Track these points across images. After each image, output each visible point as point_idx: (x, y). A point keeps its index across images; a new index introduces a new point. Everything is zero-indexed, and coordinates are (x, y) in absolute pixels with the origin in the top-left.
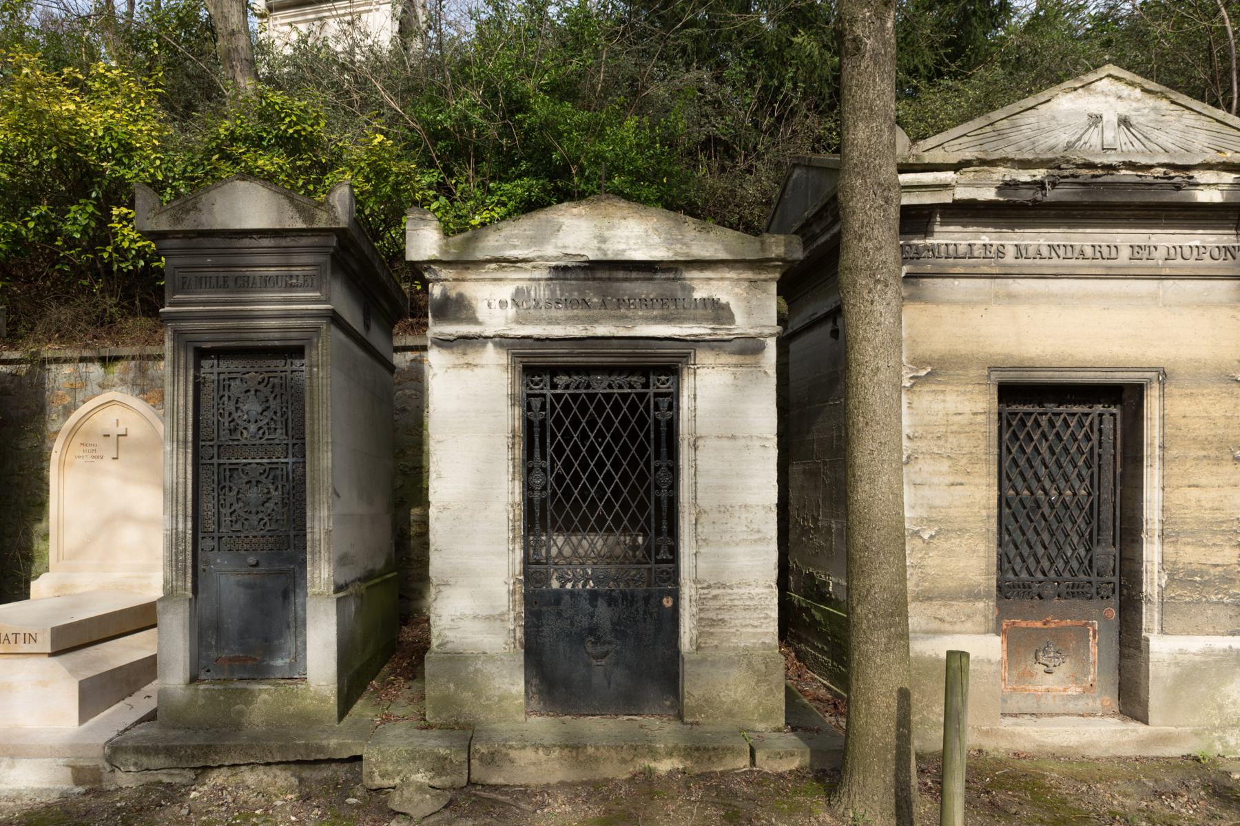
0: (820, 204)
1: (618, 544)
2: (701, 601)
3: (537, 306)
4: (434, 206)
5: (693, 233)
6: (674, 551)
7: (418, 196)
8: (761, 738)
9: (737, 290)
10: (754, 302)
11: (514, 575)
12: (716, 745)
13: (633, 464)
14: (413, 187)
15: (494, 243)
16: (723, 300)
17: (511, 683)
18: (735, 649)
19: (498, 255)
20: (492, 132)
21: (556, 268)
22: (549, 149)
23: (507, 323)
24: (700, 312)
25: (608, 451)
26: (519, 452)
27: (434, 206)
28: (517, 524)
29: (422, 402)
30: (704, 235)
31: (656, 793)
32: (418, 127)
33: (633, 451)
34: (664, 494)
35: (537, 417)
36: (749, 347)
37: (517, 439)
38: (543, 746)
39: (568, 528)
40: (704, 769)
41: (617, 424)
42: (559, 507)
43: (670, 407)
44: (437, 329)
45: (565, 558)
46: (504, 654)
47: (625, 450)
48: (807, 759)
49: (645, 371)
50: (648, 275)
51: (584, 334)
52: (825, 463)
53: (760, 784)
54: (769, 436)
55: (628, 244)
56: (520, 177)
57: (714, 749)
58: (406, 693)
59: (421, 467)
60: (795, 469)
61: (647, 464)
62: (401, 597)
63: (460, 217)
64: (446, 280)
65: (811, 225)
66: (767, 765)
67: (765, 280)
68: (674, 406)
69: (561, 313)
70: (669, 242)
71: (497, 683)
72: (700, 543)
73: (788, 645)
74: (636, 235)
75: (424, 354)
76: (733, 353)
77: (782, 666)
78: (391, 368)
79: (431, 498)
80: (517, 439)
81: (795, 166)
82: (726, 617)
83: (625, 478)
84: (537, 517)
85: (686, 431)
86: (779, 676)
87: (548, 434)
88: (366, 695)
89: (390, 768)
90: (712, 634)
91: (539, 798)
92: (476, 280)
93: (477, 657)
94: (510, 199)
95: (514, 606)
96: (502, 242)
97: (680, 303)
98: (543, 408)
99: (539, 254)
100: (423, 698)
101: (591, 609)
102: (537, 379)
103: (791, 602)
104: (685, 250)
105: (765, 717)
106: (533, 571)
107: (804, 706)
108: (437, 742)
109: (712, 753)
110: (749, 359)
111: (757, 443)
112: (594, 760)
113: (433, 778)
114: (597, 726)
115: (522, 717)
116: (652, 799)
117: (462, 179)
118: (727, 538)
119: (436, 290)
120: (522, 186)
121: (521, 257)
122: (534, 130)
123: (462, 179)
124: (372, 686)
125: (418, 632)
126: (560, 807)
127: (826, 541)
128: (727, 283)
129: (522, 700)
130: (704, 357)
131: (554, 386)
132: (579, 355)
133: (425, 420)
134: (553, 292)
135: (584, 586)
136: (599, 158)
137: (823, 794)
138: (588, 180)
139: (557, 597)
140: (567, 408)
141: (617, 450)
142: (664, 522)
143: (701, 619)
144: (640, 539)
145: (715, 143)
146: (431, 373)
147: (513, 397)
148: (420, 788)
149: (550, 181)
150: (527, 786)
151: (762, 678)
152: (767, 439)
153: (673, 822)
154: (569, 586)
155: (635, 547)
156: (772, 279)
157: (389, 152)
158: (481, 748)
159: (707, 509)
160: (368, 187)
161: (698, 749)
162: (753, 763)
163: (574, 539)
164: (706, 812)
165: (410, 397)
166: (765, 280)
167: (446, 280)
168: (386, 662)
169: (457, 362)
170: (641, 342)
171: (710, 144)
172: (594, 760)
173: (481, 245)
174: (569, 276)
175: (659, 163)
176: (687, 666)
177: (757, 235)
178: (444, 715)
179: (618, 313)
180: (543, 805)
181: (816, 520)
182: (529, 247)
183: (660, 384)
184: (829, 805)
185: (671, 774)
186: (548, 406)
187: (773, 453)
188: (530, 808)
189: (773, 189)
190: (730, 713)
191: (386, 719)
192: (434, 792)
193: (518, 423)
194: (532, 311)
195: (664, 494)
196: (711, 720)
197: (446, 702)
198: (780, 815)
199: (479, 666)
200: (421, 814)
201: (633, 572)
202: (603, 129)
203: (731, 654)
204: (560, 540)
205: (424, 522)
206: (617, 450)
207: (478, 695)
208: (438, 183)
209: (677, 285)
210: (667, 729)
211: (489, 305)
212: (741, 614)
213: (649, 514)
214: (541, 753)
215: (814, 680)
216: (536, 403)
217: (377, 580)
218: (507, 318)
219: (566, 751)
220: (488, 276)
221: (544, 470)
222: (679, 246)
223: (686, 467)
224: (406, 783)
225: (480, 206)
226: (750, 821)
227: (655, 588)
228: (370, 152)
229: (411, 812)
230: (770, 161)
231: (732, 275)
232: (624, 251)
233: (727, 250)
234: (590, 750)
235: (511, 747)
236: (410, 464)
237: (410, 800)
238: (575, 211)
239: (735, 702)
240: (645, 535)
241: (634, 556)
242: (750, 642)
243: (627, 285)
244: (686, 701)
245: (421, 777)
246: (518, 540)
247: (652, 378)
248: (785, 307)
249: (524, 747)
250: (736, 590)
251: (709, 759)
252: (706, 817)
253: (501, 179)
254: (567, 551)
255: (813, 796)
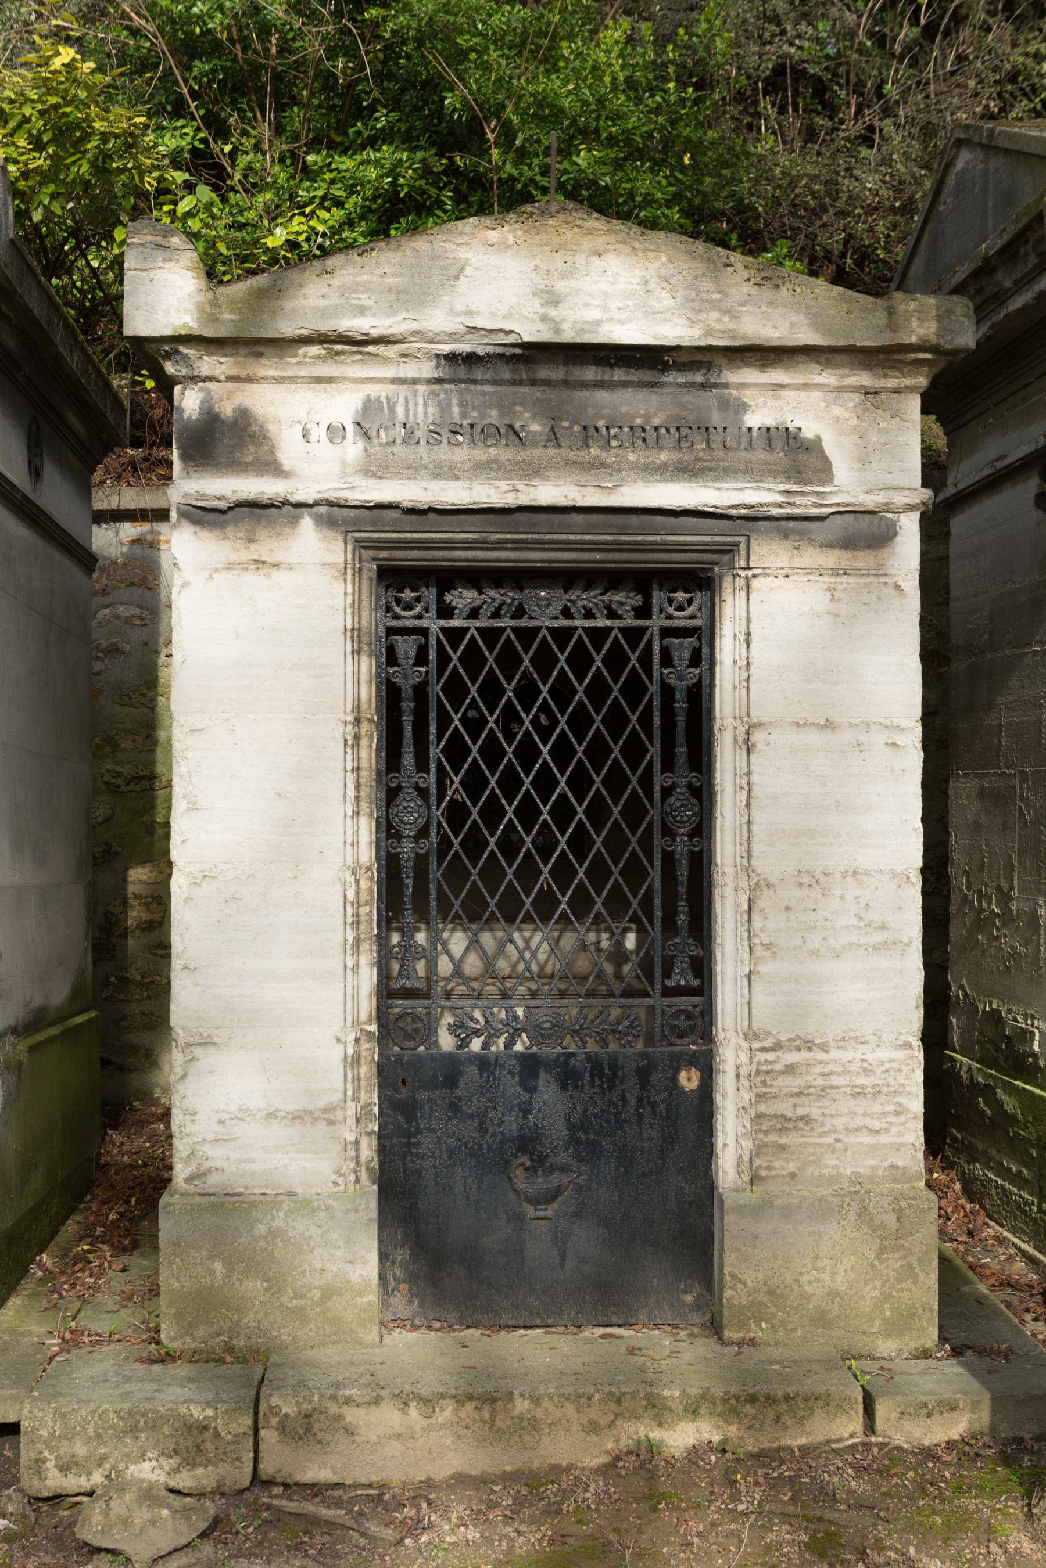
0: (1013, 229)
1: (583, 947)
2: (760, 1079)
3: (410, 437)
4: (185, 205)
5: (746, 288)
6: (702, 968)
7: (150, 182)
8: (888, 1374)
9: (837, 411)
10: (874, 437)
11: (356, 1022)
12: (791, 1390)
13: (616, 782)
14: (138, 167)
15: (318, 299)
16: (809, 433)
17: (344, 1259)
18: (831, 1180)
19: (324, 326)
20: (312, 46)
21: (452, 358)
22: (435, 86)
23: (344, 474)
24: (759, 456)
25: (562, 752)
26: (368, 754)
27: (185, 205)
28: (364, 910)
29: (155, 633)
30: (767, 293)
31: (663, 1497)
32: (151, 27)
33: (616, 753)
34: (681, 846)
35: (408, 678)
36: (863, 533)
37: (365, 727)
38: (419, 1398)
39: (474, 914)
40: (766, 1443)
41: (580, 694)
42: (455, 874)
43: (695, 659)
44: (190, 485)
45: (466, 980)
46: (335, 1196)
47: (598, 751)
48: (984, 1417)
49: (643, 581)
50: (647, 376)
51: (510, 500)
52: (1024, 776)
53: (884, 1473)
54: (904, 723)
55: (605, 308)
56: (372, 142)
57: (788, 1398)
58: (116, 1281)
59: (153, 777)
60: (963, 788)
61: (646, 781)
62: (105, 1063)
63: (239, 227)
64: (211, 379)
65: (993, 270)
66: (899, 1429)
67: (897, 391)
68: (702, 656)
69: (460, 454)
70: (696, 305)
71: (317, 1259)
72: (758, 951)
73: (948, 1166)
74: (624, 289)
75: (162, 527)
76: (830, 545)
77: (934, 1214)
78: (86, 559)
79: (175, 855)
80: (365, 727)
81: (960, 143)
82: (815, 1112)
83: (598, 812)
84: (405, 892)
85: (728, 711)
86: (925, 1238)
87: (433, 715)
88: (27, 1286)
89: (80, 1450)
90: (783, 1148)
91: (409, 1512)
92: (278, 380)
93: (274, 1203)
94: (351, 190)
95: (357, 1090)
96: (334, 300)
97: (717, 437)
98: (421, 658)
99: (415, 326)
100: (154, 1291)
101: (525, 1096)
102: (408, 595)
103: (953, 1074)
104: (728, 323)
105: (896, 1327)
106: (400, 1005)
107: (980, 1301)
108: (186, 1392)
109: (783, 1407)
110: (863, 559)
111: (879, 738)
112: (530, 1425)
113: (175, 1471)
114: (539, 1352)
115: (372, 1334)
116: (654, 1509)
117: (248, 143)
118: (815, 940)
119: (189, 402)
120: (377, 163)
121: (375, 333)
122: (404, 43)
123: (248, 143)
124: (41, 1266)
125: (142, 1143)
126: (453, 1529)
127: (1026, 942)
128: (816, 395)
129: (372, 1297)
130: (767, 553)
131: (446, 611)
132: (500, 545)
133: (163, 673)
134: (444, 409)
135: (509, 1045)
136: (546, 112)
137: (1018, 1491)
138: (522, 155)
139: (450, 1070)
140: (472, 659)
141: (580, 750)
142: (683, 907)
143: (760, 1116)
144: (630, 941)
145: (795, 80)
146: (177, 581)
147: (355, 634)
148: (148, 1495)
149: (440, 155)
150: (383, 1486)
151: (890, 1241)
152: (900, 729)
153: (697, 1559)
154: (476, 1045)
155: (619, 956)
156: (911, 389)
157: (87, 87)
158: (283, 1403)
159: (773, 879)
160: (40, 162)
161: (752, 1399)
162: (870, 1427)
163: (487, 939)
164: (770, 1537)
165: (128, 621)
166: (897, 391)
167: (211, 379)
168: (72, 1211)
169: (233, 557)
170: (634, 519)
171: (783, 79)
172: (530, 1425)
173: (288, 305)
174: (478, 374)
175: (673, 123)
176: (730, 1219)
177: (878, 294)
178: (201, 1332)
179: (583, 455)
180: (418, 1527)
181: (1005, 898)
182: (392, 310)
183: (672, 610)
184: (1030, 1516)
185: (695, 1453)
186: (432, 655)
187: (914, 760)
188: (389, 1534)
189: (917, 181)
190: (822, 1320)
191: (72, 1341)
192: (178, 1502)
193: (368, 692)
194: (398, 449)
195: (681, 846)
196: (780, 1335)
197: (205, 1303)
198: (926, 1538)
199: (279, 1222)
200: (151, 1552)
201: (615, 1013)
202: (553, 46)
203: (825, 1191)
204: (458, 941)
205: (159, 899)
206: (580, 750)
207: (275, 1285)
208: (194, 151)
209: (711, 398)
210: (687, 1356)
211: (305, 434)
212: (845, 1104)
213: (650, 890)
214: (413, 1412)
215: (1001, 1241)
216: (407, 647)
217: (53, 1031)
218: (344, 464)
219: (469, 1407)
220: (303, 372)
221: (423, 793)
222: (714, 315)
223: (729, 788)
224: (115, 1482)
225: (292, 203)
226: (862, 1555)
227: (661, 1050)
228: (46, 85)
229: (128, 1548)
230: (911, 121)
231: (828, 377)
232: (598, 323)
233: (817, 326)
234: (522, 1405)
235: (349, 1401)
236: (127, 770)
237: (125, 1522)
238: (493, 235)
239: (834, 1294)
240: (641, 931)
241: (618, 976)
242: (865, 1165)
243: (602, 396)
244: (728, 1293)
245: (150, 1471)
246: (365, 946)
247: (658, 597)
248: (941, 442)
249: (377, 1401)
250: (834, 1054)
251: (777, 1419)
252: (768, 1548)
253: (332, 147)
254: (473, 965)
255: (994, 1495)
